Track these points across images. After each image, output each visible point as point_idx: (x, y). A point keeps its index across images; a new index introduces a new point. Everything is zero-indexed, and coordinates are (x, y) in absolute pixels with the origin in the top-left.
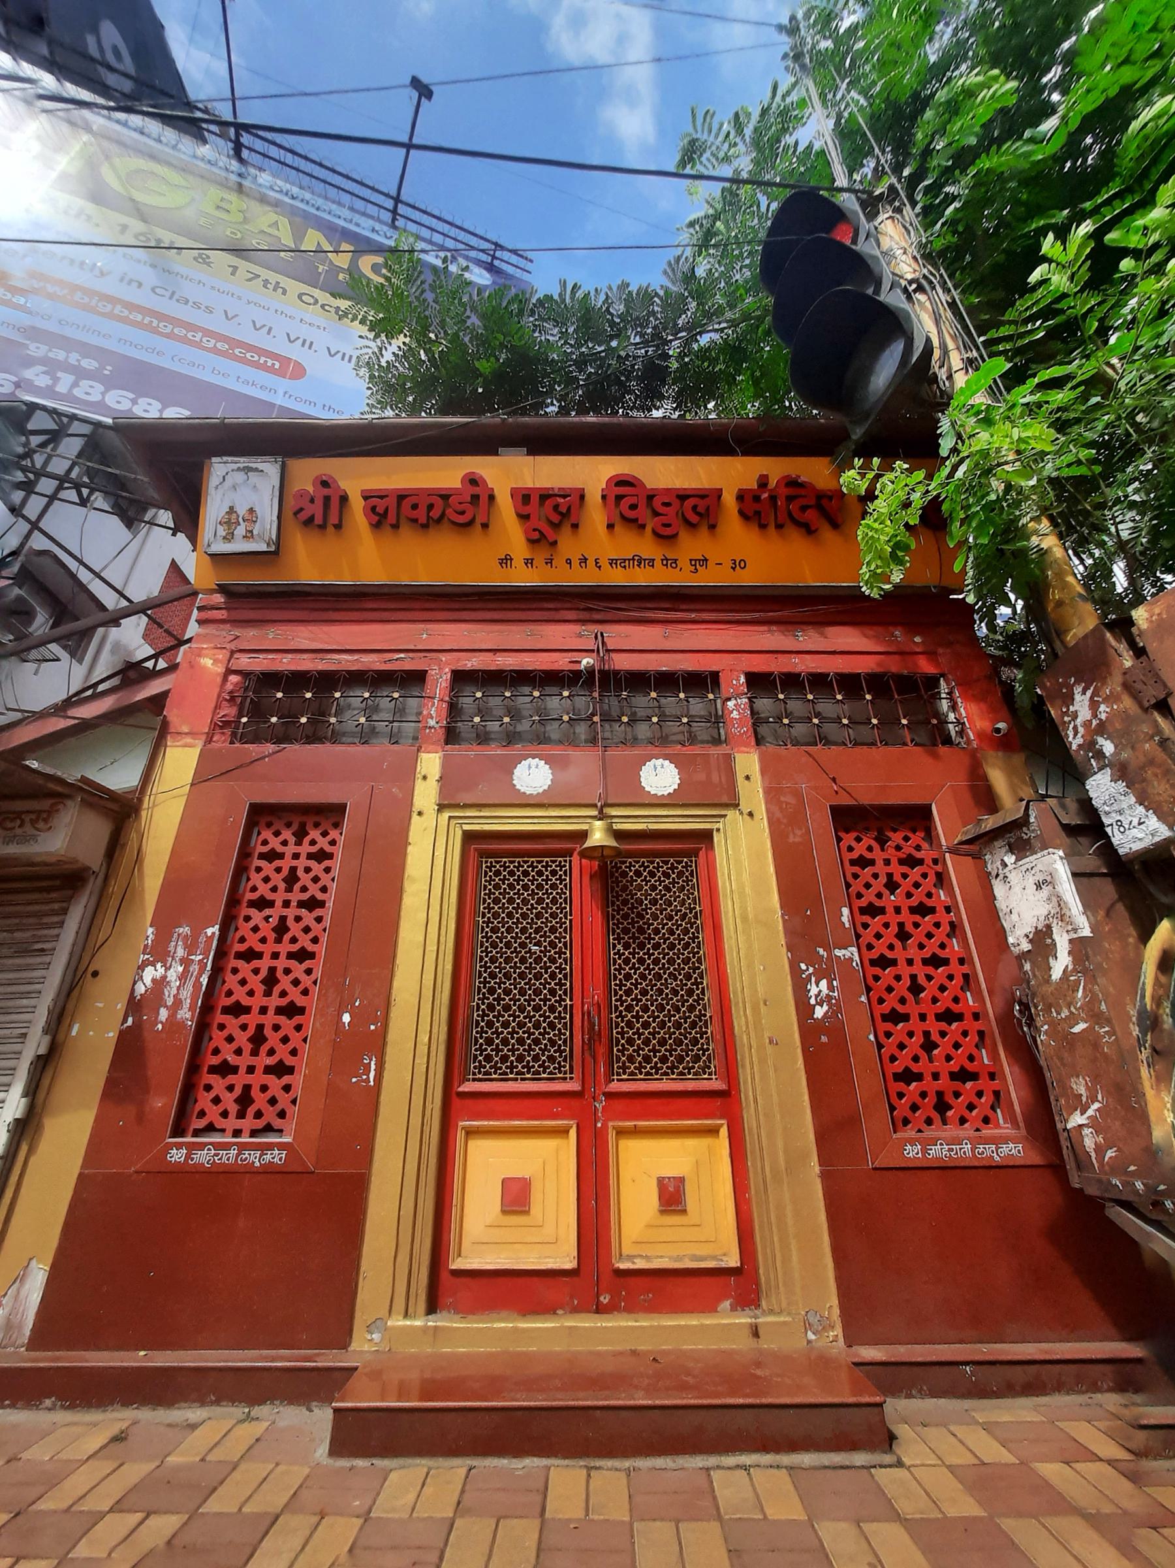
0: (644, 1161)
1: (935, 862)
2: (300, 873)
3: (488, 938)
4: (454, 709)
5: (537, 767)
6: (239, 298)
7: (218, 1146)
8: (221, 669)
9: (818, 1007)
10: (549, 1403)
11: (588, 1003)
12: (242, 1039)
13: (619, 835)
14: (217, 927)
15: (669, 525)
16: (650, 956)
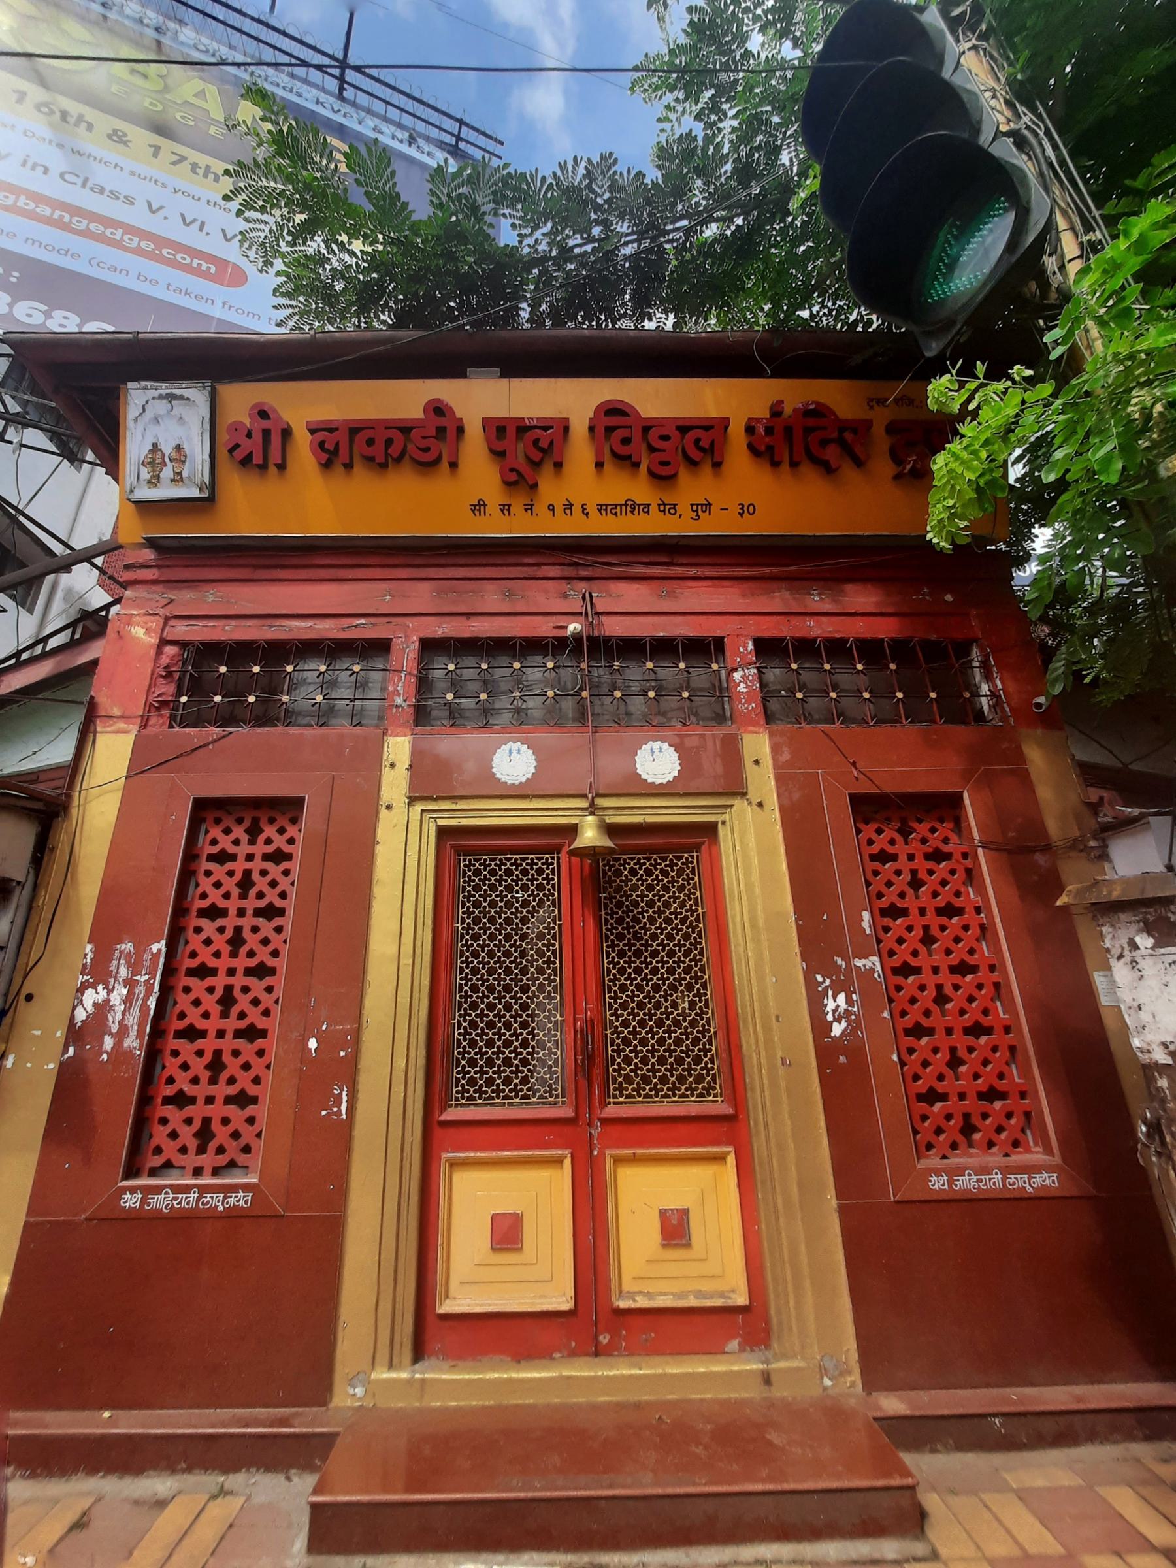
0: (643, 1190)
1: (965, 856)
2: (255, 876)
3: (468, 947)
4: (423, 684)
6: (164, 186)
7: (177, 1189)
8: (154, 640)
9: (835, 1025)
10: (548, 1494)
11: (580, 1019)
12: (199, 1066)
13: (611, 830)
14: (163, 942)
16: (647, 964)
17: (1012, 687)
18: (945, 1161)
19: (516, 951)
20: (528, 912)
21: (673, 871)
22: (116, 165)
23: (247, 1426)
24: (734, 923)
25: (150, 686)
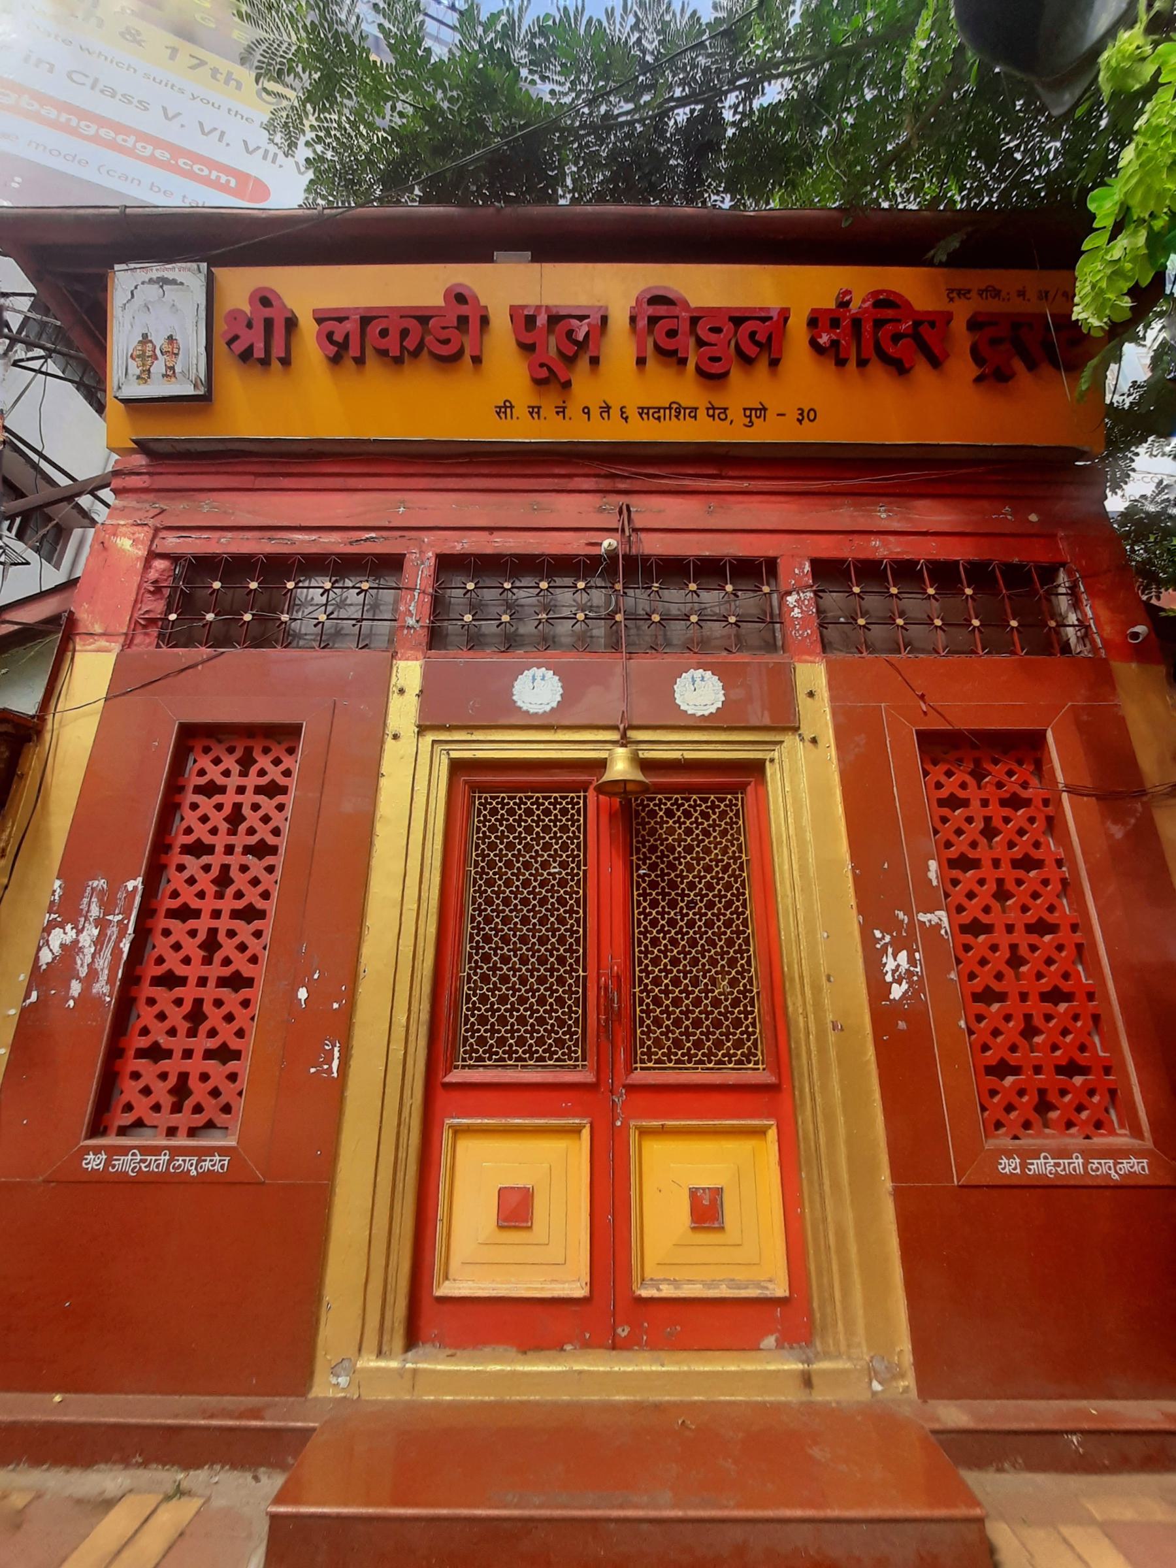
0: (672, 1166)
1: (1046, 802)
2: (246, 811)
4: (438, 605)
5: (543, 678)
6: (182, 91)
7: (146, 1150)
8: (142, 552)
9: (895, 986)
11: (604, 975)
12: (176, 1016)
13: (646, 766)
14: (140, 879)
15: (718, 359)
16: (683, 916)
17: (1104, 614)
18: (1017, 1142)
19: (534, 899)
20: (549, 856)
21: (714, 813)
22: (129, 66)
23: (212, 1416)
24: (782, 873)
25: (136, 601)
